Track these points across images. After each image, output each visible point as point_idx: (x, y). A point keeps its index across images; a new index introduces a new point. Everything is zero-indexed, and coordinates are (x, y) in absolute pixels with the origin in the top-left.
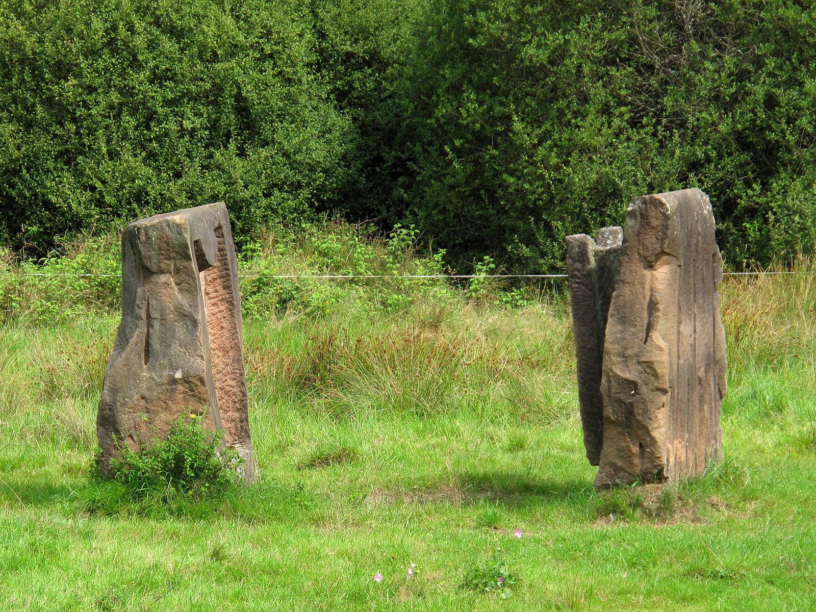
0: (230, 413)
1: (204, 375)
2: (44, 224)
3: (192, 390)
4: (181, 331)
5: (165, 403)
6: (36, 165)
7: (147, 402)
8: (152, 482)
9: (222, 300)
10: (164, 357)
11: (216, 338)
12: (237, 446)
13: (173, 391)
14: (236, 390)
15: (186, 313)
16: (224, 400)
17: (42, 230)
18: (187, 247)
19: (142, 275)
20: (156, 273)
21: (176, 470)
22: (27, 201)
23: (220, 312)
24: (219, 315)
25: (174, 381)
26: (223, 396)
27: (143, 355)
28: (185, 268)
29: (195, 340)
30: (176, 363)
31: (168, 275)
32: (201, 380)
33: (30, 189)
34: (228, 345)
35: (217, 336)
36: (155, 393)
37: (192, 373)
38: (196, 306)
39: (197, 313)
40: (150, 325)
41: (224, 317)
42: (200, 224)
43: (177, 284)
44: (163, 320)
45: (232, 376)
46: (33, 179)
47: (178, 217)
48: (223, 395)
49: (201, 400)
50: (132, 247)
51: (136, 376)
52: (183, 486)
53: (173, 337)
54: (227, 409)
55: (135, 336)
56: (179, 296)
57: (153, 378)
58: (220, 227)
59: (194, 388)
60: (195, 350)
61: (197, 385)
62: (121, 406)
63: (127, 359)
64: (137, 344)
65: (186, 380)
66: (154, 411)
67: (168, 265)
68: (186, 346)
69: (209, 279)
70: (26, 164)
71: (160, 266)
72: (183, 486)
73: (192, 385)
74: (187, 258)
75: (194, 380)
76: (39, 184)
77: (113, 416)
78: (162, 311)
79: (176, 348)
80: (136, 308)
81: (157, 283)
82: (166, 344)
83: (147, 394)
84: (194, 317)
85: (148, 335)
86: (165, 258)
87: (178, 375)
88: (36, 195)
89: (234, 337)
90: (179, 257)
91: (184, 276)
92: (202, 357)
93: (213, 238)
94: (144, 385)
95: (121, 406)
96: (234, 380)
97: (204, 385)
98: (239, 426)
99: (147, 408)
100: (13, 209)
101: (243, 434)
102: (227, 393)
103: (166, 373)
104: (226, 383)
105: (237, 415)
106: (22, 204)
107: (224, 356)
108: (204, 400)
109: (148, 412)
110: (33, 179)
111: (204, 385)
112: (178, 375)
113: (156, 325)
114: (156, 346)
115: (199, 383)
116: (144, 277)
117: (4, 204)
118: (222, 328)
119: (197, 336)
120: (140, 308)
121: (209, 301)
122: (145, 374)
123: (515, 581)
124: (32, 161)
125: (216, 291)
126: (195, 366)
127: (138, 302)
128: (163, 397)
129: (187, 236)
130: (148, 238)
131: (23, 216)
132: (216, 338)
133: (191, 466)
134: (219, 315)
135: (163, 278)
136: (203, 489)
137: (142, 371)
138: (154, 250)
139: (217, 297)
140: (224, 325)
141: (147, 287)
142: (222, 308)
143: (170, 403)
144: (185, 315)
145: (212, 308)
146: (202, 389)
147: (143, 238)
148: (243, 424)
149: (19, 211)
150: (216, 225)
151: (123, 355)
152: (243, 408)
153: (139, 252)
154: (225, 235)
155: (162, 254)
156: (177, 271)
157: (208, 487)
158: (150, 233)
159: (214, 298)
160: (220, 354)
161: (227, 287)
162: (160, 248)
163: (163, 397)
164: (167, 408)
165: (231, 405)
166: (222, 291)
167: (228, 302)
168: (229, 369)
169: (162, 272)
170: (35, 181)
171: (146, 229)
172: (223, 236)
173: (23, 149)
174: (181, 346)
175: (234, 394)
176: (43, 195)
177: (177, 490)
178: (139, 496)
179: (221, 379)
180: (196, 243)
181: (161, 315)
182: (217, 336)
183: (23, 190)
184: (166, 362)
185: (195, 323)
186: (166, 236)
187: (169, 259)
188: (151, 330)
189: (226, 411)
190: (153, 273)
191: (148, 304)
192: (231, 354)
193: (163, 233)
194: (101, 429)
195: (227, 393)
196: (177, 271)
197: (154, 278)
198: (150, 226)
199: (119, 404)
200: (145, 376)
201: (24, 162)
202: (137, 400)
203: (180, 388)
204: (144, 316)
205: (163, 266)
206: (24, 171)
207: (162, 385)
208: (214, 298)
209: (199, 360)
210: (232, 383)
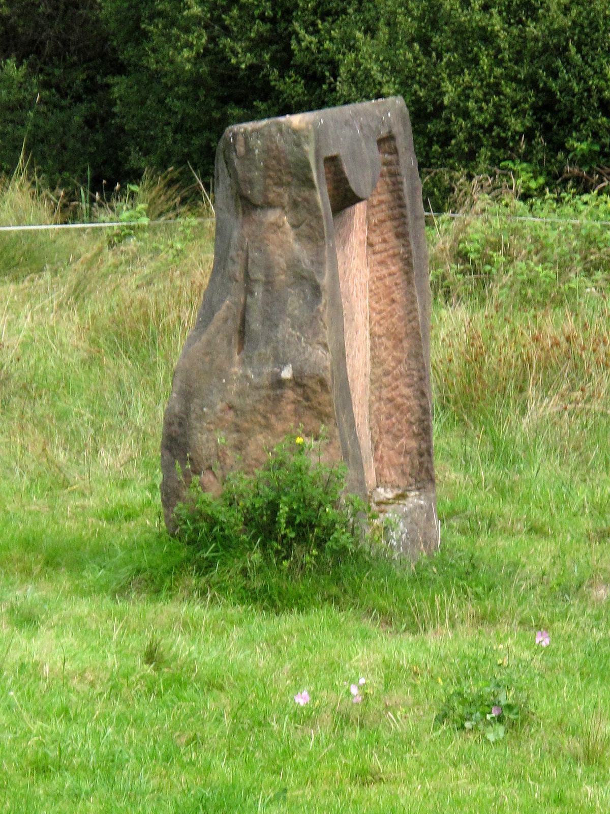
0: (403, 440)
1: (328, 376)
2: (600, 138)
3: (307, 399)
4: (294, 303)
5: (265, 417)
6: (592, 40)
7: (237, 415)
8: (226, 543)
9: (394, 256)
10: (267, 343)
11: (383, 318)
12: (413, 494)
13: (278, 399)
14: (413, 403)
15: (305, 274)
16: (394, 420)
17: (597, 148)
18: (307, 166)
19: (240, 210)
20: (262, 207)
21: (263, 526)
22: (575, 100)
23: (390, 275)
24: (388, 281)
25: (279, 383)
26: (392, 411)
27: (235, 339)
28: (306, 200)
29: (315, 317)
30: (284, 353)
31: (278, 212)
32: (322, 383)
33: (581, 79)
34: (401, 328)
35: (384, 314)
36: (249, 401)
37: (307, 370)
38: (321, 264)
39: (321, 273)
40: (249, 292)
41: (396, 284)
42: (347, 132)
43: (294, 226)
44: (269, 283)
45: (407, 380)
46: (587, 63)
47: (296, 120)
48: (392, 411)
49: (322, 416)
50: (227, 163)
51: (221, 372)
52: (277, 552)
53: (282, 311)
54: (399, 434)
55: (224, 307)
56: (296, 246)
57: (247, 377)
58: (390, 138)
59: (311, 396)
60: (316, 334)
61: (314, 392)
62: (196, 419)
63: (209, 343)
64: (226, 320)
65: (298, 382)
66: (247, 431)
67: (279, 195)
68: (300, 328)
69: (374, 220)
70: (576, 38)
71: (266, 197)
72: (277, 552)
73: (308, 391)
74: (308, 183)
75: (311, 383)
76: (596, 72)
77: (184, 435)
78: (268, 269)
79: (285, 330)
80: (230, 262)
81: (262, 223)
82: (270, 322)
83: (236, 401)
84: (315, 281)
85: (245, 309)
86: (276, 184)
87: (287, 373)
88: (589, 90)
89: (411, 317)
90: (295, 182)
91: (303, 214)
92: (325, 346)
93: (373, 154)
94: (234, 387)
95: (196, 419)
96: (409, 386)
97: (327, 392)
98: (416, 462)
99: (236, 425)
100: (555, 113)
101: (423, 475)
102: (398, 407)
103: (267, 370)
104: (397, 392)
105: (413, 444)
106: (568, 104)
107: (395, 347)
108: (328, 416)
109: (238, 431)
110: (587, 63)
111: (327, 392)
112: (287, 373)
113: (259, 291)
114: (255, 325)
115: (319, 389)
116: (244, 213)
117: (540, 103)
118: (393, 301)
119: (318, 311)
120: (234, 262)
121: (373, 257)
122: (236, 369)
123: (517, 714)
124: (587, 35)
125: (385, 241)
126: (313, 359)
127: (233, 253)
128: (261, 407)
129: (309, 149)
130: (249, 150)
131: (567, 123)
132: (383, 318)
133: (290, 522)
134: (388, 281)
135: (272, 216)
136: (308, 558)
137: (231, 364)
138: (257, 168)
139: (386, 250)
140: (397, 296)
141: (246, 229)
142: (393, 269)
143: (273, 419)
144: (303, 277)
145: (379, 268)
146: (324, 397)
147: (241, 149)
148: (422, 459)
149: (564, 115)
150: (384, 133)
151: (204, 338)
152: (425, 432)
153: (235, 171)
154: (401, 150)
155: (270, 177)
156: (295, 205)
157: (317, 557)
158: (252, 141)
159: (381, 252)
160: (389, 344)
161: (401, 235)
162: (267, 167)
163: (261, 407)
164: (268, 427)
165: (405, 427)
166: (394, 241)
167: (402, 259)
168: (402, 368)
169: (270, 205)
170: (590, 66)
171: (246, 135)
172: (395, 151)
173: (574, 12)
174: (293, 327)
175: (409, 409)
176: (600, 91)
177: (266, 556)
178: (205, 567)
179: (390, 385)
180: (333, 162)
181: (267, 276)
182: (384, 314)
183: (569, 80)
184: (269, 351)
185: (317, 290)
186: (277, 147)
187: (280, 184)
188: (249, 300)
189: (396, 438)
190: (255, 207)
191: (247, 258)
192: (406, 344)
193: (272, 142)
194: (167, 453)
195: (398, 407)
196: (295, 205)
197: (258, 215)
198: (253, 131)
199: (193, 416)
200: (236, 373)
201: (574, 34)
202: (222, 411)
203: (290, 394)
204: (240, 276)
205: (271, 196)
206: (573, 50)
207: (261, 387)
208: (381, 252)
209: (320, 352)
210: (406, 391)
